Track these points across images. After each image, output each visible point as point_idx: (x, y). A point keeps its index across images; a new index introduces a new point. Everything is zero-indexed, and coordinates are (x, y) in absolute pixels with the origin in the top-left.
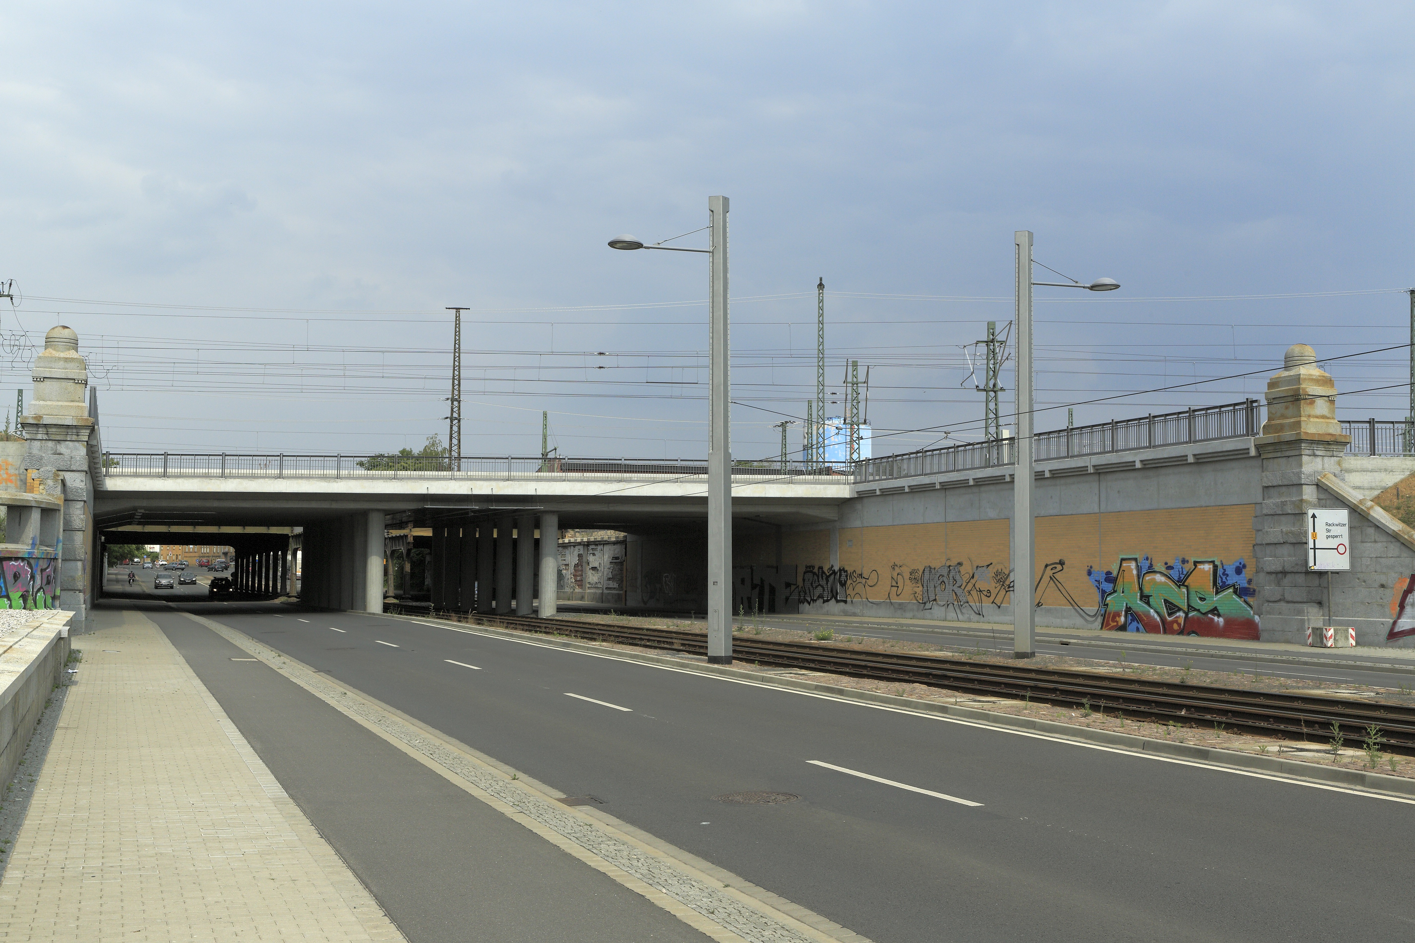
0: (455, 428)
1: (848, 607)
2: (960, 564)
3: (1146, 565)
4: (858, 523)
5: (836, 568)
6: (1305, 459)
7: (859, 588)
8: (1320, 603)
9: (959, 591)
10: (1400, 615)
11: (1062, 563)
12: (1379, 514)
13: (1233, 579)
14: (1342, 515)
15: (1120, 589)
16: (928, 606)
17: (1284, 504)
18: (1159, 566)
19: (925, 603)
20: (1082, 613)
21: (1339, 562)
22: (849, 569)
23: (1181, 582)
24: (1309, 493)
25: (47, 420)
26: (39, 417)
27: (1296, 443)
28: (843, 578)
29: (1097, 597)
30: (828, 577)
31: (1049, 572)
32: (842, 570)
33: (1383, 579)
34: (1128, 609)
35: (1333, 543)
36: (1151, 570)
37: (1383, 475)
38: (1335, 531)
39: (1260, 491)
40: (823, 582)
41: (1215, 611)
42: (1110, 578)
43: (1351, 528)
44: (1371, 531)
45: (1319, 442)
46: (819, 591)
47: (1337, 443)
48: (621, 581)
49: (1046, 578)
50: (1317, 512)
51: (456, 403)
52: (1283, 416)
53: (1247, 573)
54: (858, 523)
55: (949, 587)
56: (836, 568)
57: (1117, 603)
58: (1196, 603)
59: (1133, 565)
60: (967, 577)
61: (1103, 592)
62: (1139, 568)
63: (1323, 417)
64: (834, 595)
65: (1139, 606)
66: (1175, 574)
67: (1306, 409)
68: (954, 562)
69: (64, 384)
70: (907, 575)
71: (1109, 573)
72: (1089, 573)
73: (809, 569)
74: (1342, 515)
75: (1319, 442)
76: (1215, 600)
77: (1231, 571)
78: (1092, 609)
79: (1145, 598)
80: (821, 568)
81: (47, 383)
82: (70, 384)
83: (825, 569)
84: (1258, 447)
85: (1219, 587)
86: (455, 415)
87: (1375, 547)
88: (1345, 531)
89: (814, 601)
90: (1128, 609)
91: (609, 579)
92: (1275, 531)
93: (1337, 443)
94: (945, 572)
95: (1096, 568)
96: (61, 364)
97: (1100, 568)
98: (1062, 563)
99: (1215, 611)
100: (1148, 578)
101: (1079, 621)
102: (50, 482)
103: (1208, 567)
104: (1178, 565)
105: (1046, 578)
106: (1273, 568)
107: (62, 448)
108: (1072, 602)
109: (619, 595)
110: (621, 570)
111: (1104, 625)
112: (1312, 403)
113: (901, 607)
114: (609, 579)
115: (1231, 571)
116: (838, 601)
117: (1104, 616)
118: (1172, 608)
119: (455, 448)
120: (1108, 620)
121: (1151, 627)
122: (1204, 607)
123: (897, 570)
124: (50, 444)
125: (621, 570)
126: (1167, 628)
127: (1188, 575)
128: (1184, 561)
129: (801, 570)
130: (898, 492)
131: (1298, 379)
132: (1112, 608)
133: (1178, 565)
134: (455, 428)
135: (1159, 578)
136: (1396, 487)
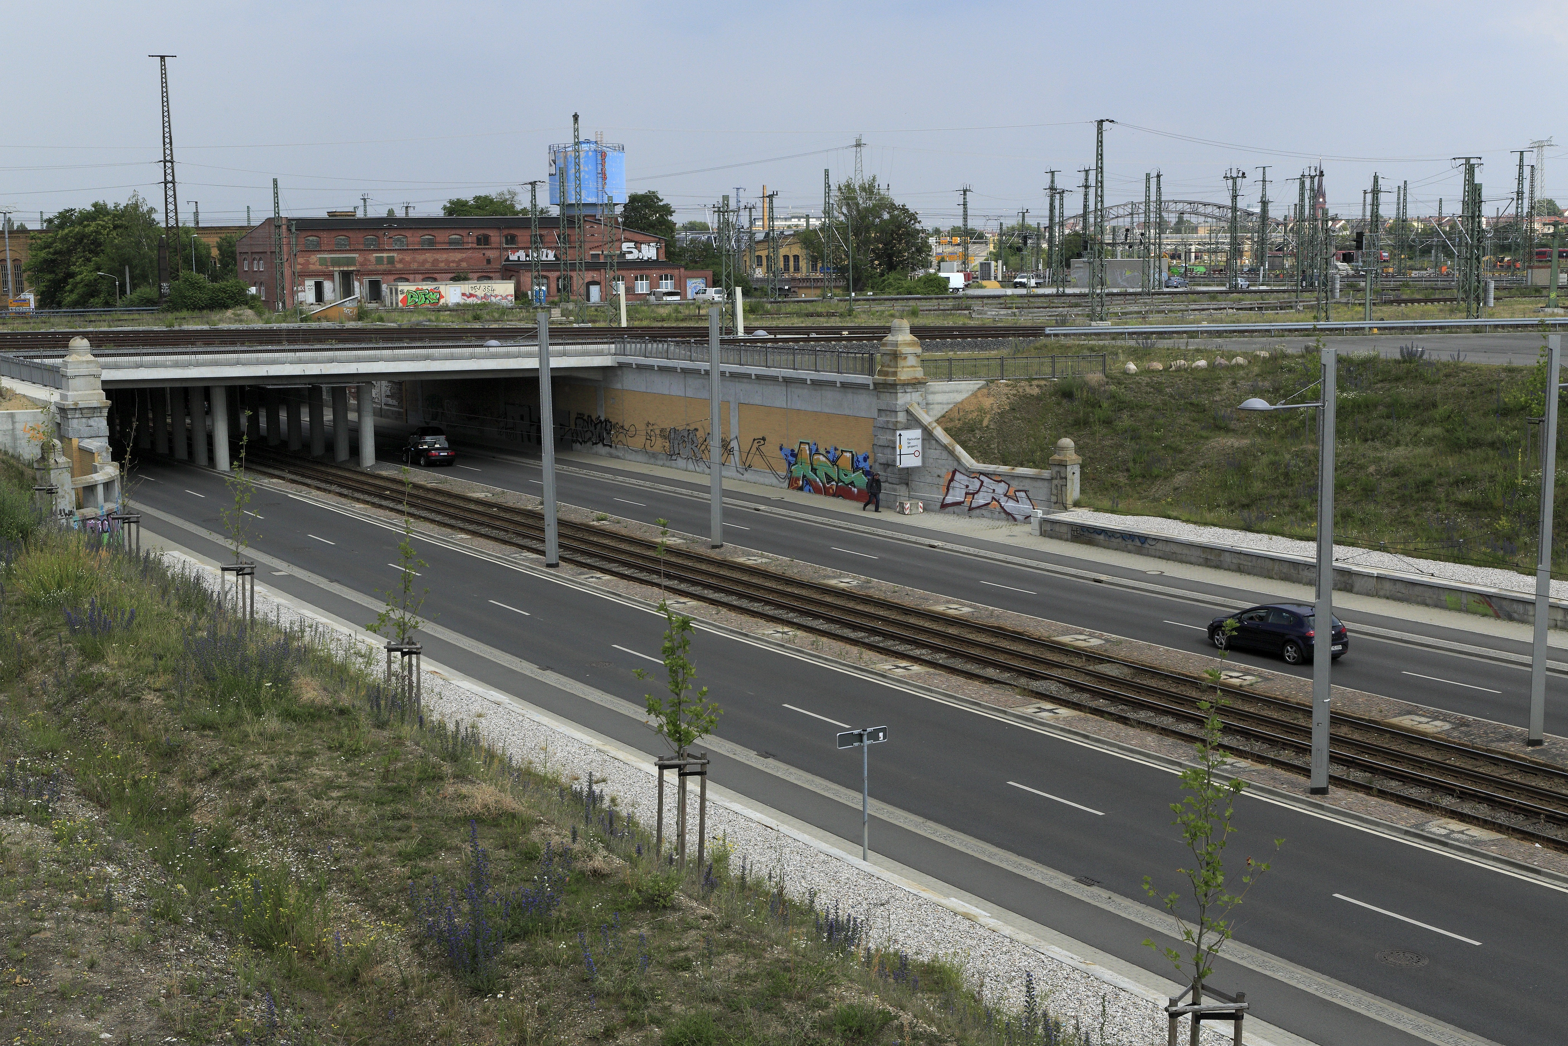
0: (170, 193)
1: (613, 451)
2: (696, 430)
3: (814, 448)
4: (619, 386)
5: (603, 419)
6: (899, 395)
7: (621, 437)
8: (907, 484)
9: (696, 450)
10: (946, 495)
11: (764, 439)
12: (939, 432)
13: (862, 465)
14: (917, 433)
15: (799, 460)
16: (674, 457)
17: (888, 422)
18: (822, 451)
19: (672, 455)
20: (777, 476)
21: (915, 462)
22: (614, 421)
23: (834, 462)
24: (902, 417)
25: (82, 405)
26: (76, 404)
27: (894, 385)
28: (608, 427)
29: (786, 466)
30: (596, 425)
31: (756, 445)
32: (607, 421)
33: (939, 472)
34: (804, 476)
35: (912, 450)
36: (817, 452)
37: (955, 394)
38: (913, 443)
39: (876, 411)
40: (592, 429)
41: (852, 483)
42: (794, 454)
43: (923, 440)
44: (934, 442)
45: (908, 384)
46: (589, 435)
47: (920, 383)
48: (400, 400)
49: (754, 449)
50: (902, 432)
51: (169, 164)
52: (889, 366)
53: (870, 462)
54: (619, 386)
55: (689, 446)
56: (603, 419)
57: (799, 471)
58: (843, 477)
59: (807, 447)
60: (700, 441)
61: (790, 463)
62: (810, 450)
63: (912, 367)
64: (601, 440)
65: (811, 475)
66: (830, 456)
67: (901, 363)
68: (692, 428)
69: (88, 378)
70: (658, 432)
71: (793, 450)
72: (781, 449)
73: (580, 416)
74: (917, 433)
75: (908, 384)
76: (853, 476)
77: (861, 459)
78: (783, 473)
79: (814, 470)
80: (589, 416)
81: (77, 379)
82: (92, 378)
83: (594, 418)
84: (875, 384)
85: (855, 469)
86: (169, 178)
87: (934, 453)
88: (919, 442)
89: (585, 442)
90: (804, 476)
91: (387, 396)
92: (884, 438)
93: (920, 383)
94: (686, 434)
95: (785, 446)
96: (85, 365)
97: (787, 447)
98: (764, 439)
99: (852, 483)
100: (816, 457)
101: (774, 481)
102: (104, 454)
103: (848, 455)
104: (832, 451)
105: (754, 449)
106: (882, 461)
107: (92, 422)
108: (771, 468)
109: (399, 413)
110: (401, 390)
111: (790, 486)
112: (905, 358)
113: (654, 456)
114: (387, 396)
115: (861, 459)
116: (604, 445)
117: (790, 479)
118: (829, 479)
119: (171, 214)
120: (793, 483)
121: (817, 490)
122: (847, 480)
123: (650, 427)
124: (84, 420)
125: (401, 390)
126: (826, 492)
127: (838, 458)
128: (836, 449)
129: (573, 416)
130: (650, 368)
131: (896, 344)
132: (795, 474)
133: (832, 451)
134: (170, 193)
135: (822, 458)
136: (962, 403)
